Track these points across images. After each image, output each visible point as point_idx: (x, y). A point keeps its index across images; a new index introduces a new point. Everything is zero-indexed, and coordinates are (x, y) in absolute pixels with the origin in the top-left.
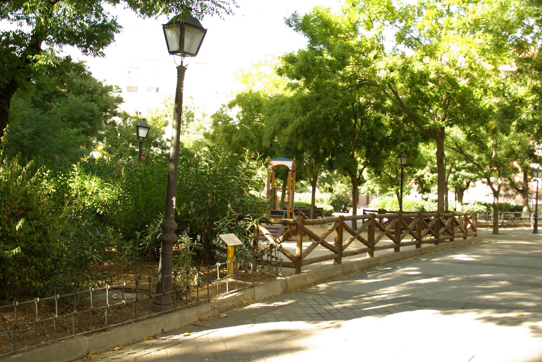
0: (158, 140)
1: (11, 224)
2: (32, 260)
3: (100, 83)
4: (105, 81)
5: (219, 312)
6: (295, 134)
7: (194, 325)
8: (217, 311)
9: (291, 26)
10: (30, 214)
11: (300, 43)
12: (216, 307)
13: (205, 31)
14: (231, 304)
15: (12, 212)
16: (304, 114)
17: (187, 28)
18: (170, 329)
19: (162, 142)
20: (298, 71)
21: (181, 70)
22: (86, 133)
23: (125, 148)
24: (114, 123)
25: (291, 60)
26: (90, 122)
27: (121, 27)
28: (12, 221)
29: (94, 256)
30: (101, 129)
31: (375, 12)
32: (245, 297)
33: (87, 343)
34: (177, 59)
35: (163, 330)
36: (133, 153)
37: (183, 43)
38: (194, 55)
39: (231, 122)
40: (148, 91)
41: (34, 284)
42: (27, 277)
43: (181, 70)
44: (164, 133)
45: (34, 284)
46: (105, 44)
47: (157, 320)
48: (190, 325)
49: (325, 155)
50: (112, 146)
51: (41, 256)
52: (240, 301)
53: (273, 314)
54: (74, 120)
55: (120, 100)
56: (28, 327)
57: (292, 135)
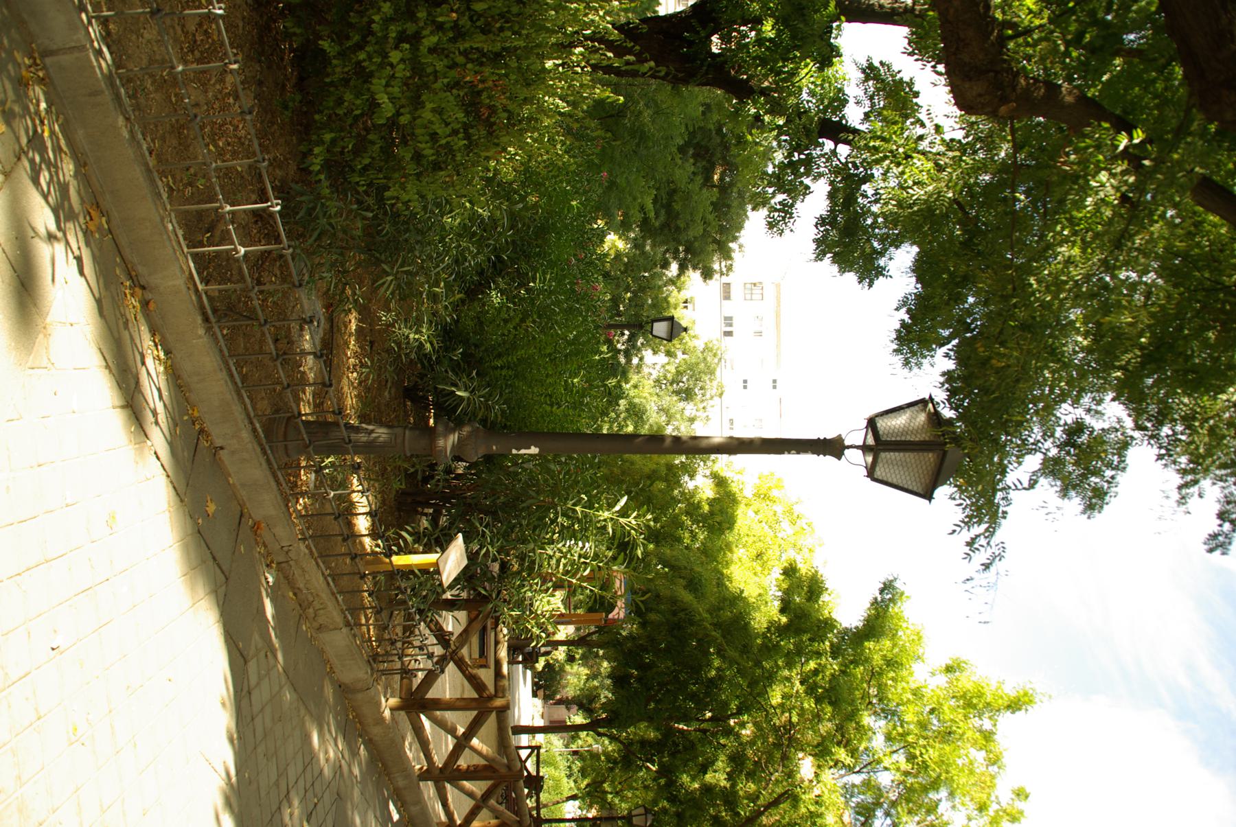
0: (640, 341)
1: (454, 91)
2: (373, 143)
3: (735, 239)
4: (741, 246)
5: (279, 563)
6: (677, 607)
7: (242, 515)
8: (281, 559)
9: (882, 591)
10: (479, 133)
11: (846, 608)
12: (292, 555)
13: (928, 495)
14: (301, 586)
15: (482, 91)
16: (717, 625)
17: (931, 457)
18: (226, 462)
19: (639, 350)
20: (799, 611)
21: (832, 447)
22: (645, 224)
23: (623, 285)
24: (666, 265)
25: (814, 588)
26: (666, 225)
27: (870, 286)
28: (462, 94)
29: (390, 278)
30: (653, 246)
31: (926, 757)
32: (322, 612)
33: (171, 283)
34: (856, 436)
35: (222, 448)
36: (616, 301)
37: (899, 450)
38: (871, 474)
39: (686, 478)
40: (726, 319)
41: (317, 150)
42: (333, 135)
43: (832, 447)
44: (655, 353)
45: (317, 150)
46: (838, 259)
47: (246, 435)
48: (242, 506)
49: (642, 667)
50: (626, 264)
51: (387, 162)
52: (310, 604)
53: (281, 688)
54: (668, 199)
55: (707, 274)
56: (216, 146)
57: (674, 601)
